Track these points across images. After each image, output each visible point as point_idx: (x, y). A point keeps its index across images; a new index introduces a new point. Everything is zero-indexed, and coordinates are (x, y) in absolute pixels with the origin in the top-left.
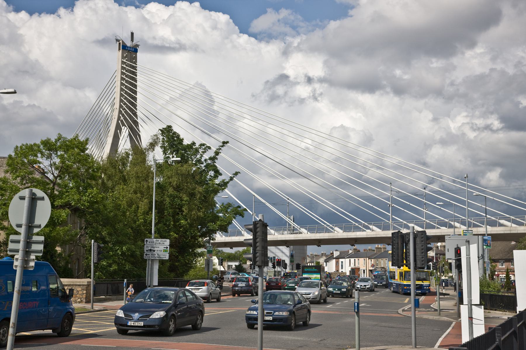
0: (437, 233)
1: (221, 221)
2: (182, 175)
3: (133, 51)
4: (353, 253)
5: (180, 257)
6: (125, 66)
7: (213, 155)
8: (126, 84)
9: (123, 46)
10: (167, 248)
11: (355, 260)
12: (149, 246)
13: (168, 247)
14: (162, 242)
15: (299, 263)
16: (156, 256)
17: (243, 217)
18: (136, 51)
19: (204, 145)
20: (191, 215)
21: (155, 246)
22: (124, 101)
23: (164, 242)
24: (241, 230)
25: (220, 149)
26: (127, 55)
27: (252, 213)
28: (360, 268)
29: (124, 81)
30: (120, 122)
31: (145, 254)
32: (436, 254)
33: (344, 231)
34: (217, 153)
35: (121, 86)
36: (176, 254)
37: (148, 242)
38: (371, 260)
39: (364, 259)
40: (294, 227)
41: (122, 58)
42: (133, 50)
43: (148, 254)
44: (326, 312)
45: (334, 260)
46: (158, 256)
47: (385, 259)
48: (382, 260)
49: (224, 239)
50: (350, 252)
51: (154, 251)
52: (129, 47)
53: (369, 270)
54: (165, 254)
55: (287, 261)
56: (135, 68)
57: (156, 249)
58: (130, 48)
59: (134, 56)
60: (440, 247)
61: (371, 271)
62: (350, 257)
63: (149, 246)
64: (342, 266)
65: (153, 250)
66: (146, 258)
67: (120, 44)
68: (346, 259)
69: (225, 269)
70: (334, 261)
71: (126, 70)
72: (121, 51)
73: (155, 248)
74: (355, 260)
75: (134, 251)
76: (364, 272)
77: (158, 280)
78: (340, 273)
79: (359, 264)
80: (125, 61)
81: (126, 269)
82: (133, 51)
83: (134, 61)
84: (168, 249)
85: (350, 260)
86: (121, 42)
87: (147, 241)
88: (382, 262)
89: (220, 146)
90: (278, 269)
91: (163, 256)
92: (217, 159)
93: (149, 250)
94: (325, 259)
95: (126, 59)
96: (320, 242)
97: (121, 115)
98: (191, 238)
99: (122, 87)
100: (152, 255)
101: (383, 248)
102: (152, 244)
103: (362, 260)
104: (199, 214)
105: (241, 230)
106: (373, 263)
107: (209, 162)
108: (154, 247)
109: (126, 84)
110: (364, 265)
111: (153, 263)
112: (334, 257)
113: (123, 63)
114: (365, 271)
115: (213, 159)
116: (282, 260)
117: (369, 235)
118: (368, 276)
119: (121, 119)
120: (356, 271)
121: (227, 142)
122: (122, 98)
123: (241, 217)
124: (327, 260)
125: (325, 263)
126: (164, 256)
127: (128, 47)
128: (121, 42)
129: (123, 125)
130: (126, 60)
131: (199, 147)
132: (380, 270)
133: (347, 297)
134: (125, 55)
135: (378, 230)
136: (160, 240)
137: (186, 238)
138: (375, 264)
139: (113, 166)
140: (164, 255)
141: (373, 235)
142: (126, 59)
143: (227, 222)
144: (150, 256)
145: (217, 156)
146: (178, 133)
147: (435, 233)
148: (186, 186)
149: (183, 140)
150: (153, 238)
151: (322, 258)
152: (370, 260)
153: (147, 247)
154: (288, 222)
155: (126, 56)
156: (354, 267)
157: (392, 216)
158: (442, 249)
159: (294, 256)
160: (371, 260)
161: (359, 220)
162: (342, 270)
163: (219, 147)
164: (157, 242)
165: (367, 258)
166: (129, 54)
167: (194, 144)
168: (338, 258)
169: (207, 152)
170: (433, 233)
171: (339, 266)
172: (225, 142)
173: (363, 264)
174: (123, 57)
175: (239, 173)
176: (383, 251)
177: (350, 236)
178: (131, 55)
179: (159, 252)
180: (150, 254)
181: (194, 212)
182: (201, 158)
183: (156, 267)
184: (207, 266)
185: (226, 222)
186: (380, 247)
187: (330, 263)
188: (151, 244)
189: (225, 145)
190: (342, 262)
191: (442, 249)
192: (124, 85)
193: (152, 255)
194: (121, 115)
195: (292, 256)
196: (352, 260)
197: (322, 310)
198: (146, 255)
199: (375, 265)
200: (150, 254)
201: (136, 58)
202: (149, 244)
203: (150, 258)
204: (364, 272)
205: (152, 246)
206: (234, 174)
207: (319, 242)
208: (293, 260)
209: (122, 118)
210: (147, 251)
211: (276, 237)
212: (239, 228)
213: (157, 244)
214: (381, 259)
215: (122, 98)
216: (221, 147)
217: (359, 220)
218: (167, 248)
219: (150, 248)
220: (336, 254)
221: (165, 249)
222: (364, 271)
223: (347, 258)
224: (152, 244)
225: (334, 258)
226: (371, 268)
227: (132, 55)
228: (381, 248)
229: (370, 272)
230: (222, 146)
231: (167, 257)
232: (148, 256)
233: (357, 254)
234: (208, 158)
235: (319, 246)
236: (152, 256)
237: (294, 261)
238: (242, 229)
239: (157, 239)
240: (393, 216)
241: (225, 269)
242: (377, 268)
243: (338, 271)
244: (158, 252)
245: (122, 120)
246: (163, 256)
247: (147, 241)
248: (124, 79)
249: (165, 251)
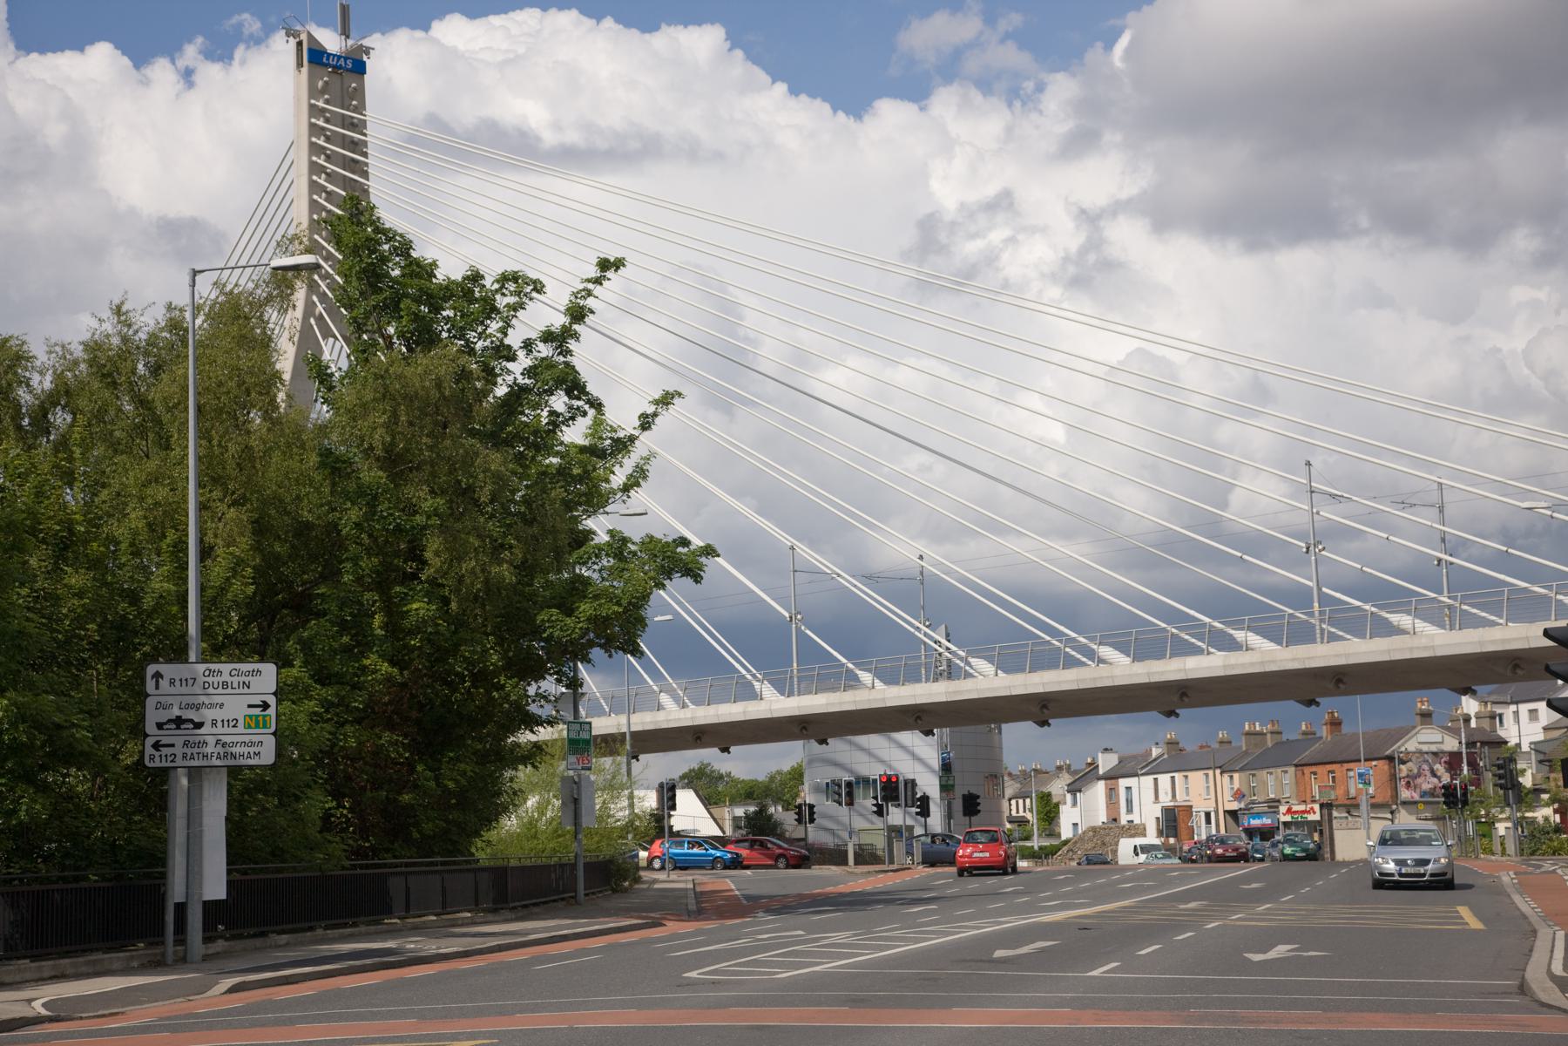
0: (1508, 641)
1: (596, 597)
2: (409, 399)
3: (348, 70)
4: (1166, 756)
5: (420, 768)
6: (321, 123)
7: (559, 320)
8: (330, 187)
9: (310, 51)
10: (265, 706)
11: (1173, 778)
12: (170, 700)
13: (272, 700)
14: (235, 680)
15: (974, 791)
16: (209, 750)
17: (697, 579)
18: (359, 68)
19: (515, 277)
20: (461, 580)
21: (203, 699)
22: (324, 248)
23: (246, 679)
24: (749, 677)
25: (589, 293)
26: (326, 82)
27: (787, 615)
28: (1191, 807)
29: (323, 176)
30: (312, 321)
31: (150, 741)
32: (1471, 744)
33: (1137, 658)
34: (578, 314)
35: (311, 193)
36: (401, 755)
37: (164, 683)
38: (1231, 777)
39: (1207, 775)
40: (949, 660)
41: (311, 96)
42: (350, 66)
43: (165, 741)
44: (1089, 1021)
45: (1101, 785)
46: (219, 749)
47: (1279, 770)
48: (1271, 773)
49: (689, 715)
50: (1155, 752)
51: (199, 725)
52: (334, 55)
53: (1225, 812)
54: (256, 739)
55: (929, 785)
56: (359, 126)
57: (208, 715)
58: (339, 57)
59: (354, 85)
60: (1478, 717)
61: (1233, 814)
62: (1155, 768)
63: (170, 700)
64: (1129, 802)
65: (191, 721)
66: (157, 764)
67: (300, 44)
68: (1141, 778)
69: (724, 832)
70: (1100, 787)
71: (325, 136)
72: (305, 70)
73: (205, 711)
74: (1173, 778)
75: (59, 727)
76: (1208, 821)
77: (229, 872)
78: (1124, 827)
79: (1188, 794)
80: (321, 104)
81: (21, 823)
82: (348, 70)
83: (354, 103)
84: (272, 711)
85: (1156, 779)
86: (304, 37)
87: (158, 676)
88: (1271, 780)
89: (589, 281)
90: (896, 816)
91: (245, 750)
92: (576, 336)
93: (170, 721)
94: (1069, 781)
95: (326, 96)
96: (1044, 706)
97: (315, 298)
98: (474, 685)
99: (315, 197)
100: (186, 744)
101: (1272, 733)
102: (184, 690)
103: (1196, 777)
104: (495, 569)
105: (749, 677)
106: (1236, 785)
107: (544, 350)
108: (197, 707)
109: (330, 187)
110: (1208, 794)
111: (201, 787)
112: (1101, 772)
113: (314, 111)
114: (1213, 816)
115: (559, 338)
116: (906, 782)
117: (1233, 666)
118: (1223, 831)
119: (317, 313)
120: (1181, 817)
121: (618, 264)
122: (316, 237)
123: (688, 581)
124: (1077, 785)
125: (1069, 797)
126: (252, 750)
127: (329, 55)
128: (304, 37)
129: (327, 334)
130: (327, 102)
131: (496, 286)
132: (1266, 809)
133: (1005, 873)
134: (320, 84)
135: (1268, 645)
136: (226, 668)
137: (450, 684)
138: (1245, 790)
139: (103, 375)
140: (252, 744)
141: (1252, 664)
142: (326, 96)
143: (624, 602)
144: (179, 750)
145: (575, 327)
146: (401, 236)
147: (1503, 641)
148: (430, 448)
149: (437, 266)
150: (192, 657)
151: (1058, 781)
152: (1226, 776)
153: (160, 706)
154: (925, 643)
155: (323, 87)
156: (1172, 804)
157: (1319, 589)
158: (1486, 724)
159: (956, 767)
160: (1231, 777)
161: (1192, 612)
162: (1130, 817)
163: (581, 287)
164: (210, 679)
165: (1218, 771)
166: (336, 78)
167: (476, 277)
168: (1111, 777)
169: (530, 306)
170: (1493, 642)
171: (1117, 803)
172: (606, 260)
173: (1203, 792)
174: (313, 92)
175: (680, 394)
176: (1270, 744)
177: (1163, 673)
178: (342, 83)
179: (226, 730)
180: (179, 741)
181: (468, 565)
182: (506, 335)
183: (215, 807)
184: (572, 806)
185: (618, 604)
186: (1258, 729)
187: (1088, 793)
188: (177, 689)
189: (610, 274)
190: (1128, 789)
191: (1486, 724)
192: (324, 189)
193: (186, 744)
194: (315, 298)
195: (946, 767)
196: (1164, 779)
197: (1062, 1003)
198: (156, 746)
199: (1246, 792)
200: (179, 741)
201: (359, 93)
202: (172, 690)
203: (179, 762)
204: (1208, 821)
205: (191, 700)
206: (656, 402)
207: (1042, 709)
208: (951, 782)
209: (320, 308)
210: (160, 726)
211: (880, 696)
212: (744, 672)
213: (211, 690)
214: (1265, 772)
215: (316, 237)
216: (590, 286)
217: (1192, 612)
218: (265, 706)
219: (176, 712)
220: (1106, 763)
221: (257, 711)
222: (1208, 815)
223: (1143, 775)
224: (184, 690)
225: (1099, 779)
226: (1234, 806)
227: (345, 86)
228: (1261, 734)
229: (1228, 817)
230: (598, 281)
231: (267, 756)
232: (165, 751)
233: (1178, 760)
234: (534, 335)
235: (1043, 723)
236: (189, 751)
237: (953, 786)
238: (754, 676)
239: (213, 666)
240: (1324, 589)
241: (724, 832)
242: (1253, 802)
243: (1115, 820)
244: (219, 730)
245: (321, 314)
246: (245, 750)
247: (158, 676)
248: (322, 169)
249: (254, 723)
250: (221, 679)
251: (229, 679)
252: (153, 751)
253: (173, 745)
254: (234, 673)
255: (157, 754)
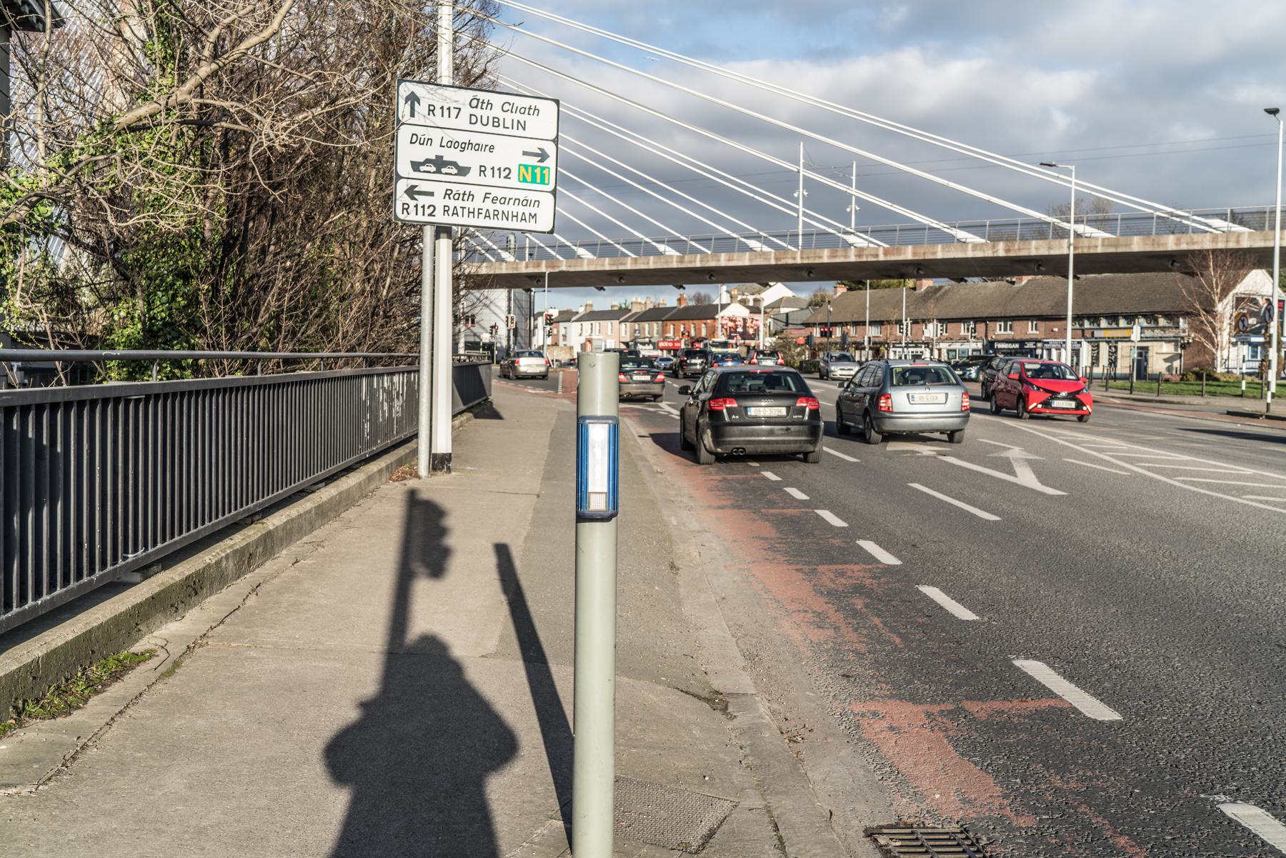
65: (454, 164)
93: (428, 161)
210: (416, 166)
232: (422, 200)
250: (491, 114)
251: (501, 115)
252: (407, 199)
253: (432, 194)
254: (507, 107)
255: (412, 203)
